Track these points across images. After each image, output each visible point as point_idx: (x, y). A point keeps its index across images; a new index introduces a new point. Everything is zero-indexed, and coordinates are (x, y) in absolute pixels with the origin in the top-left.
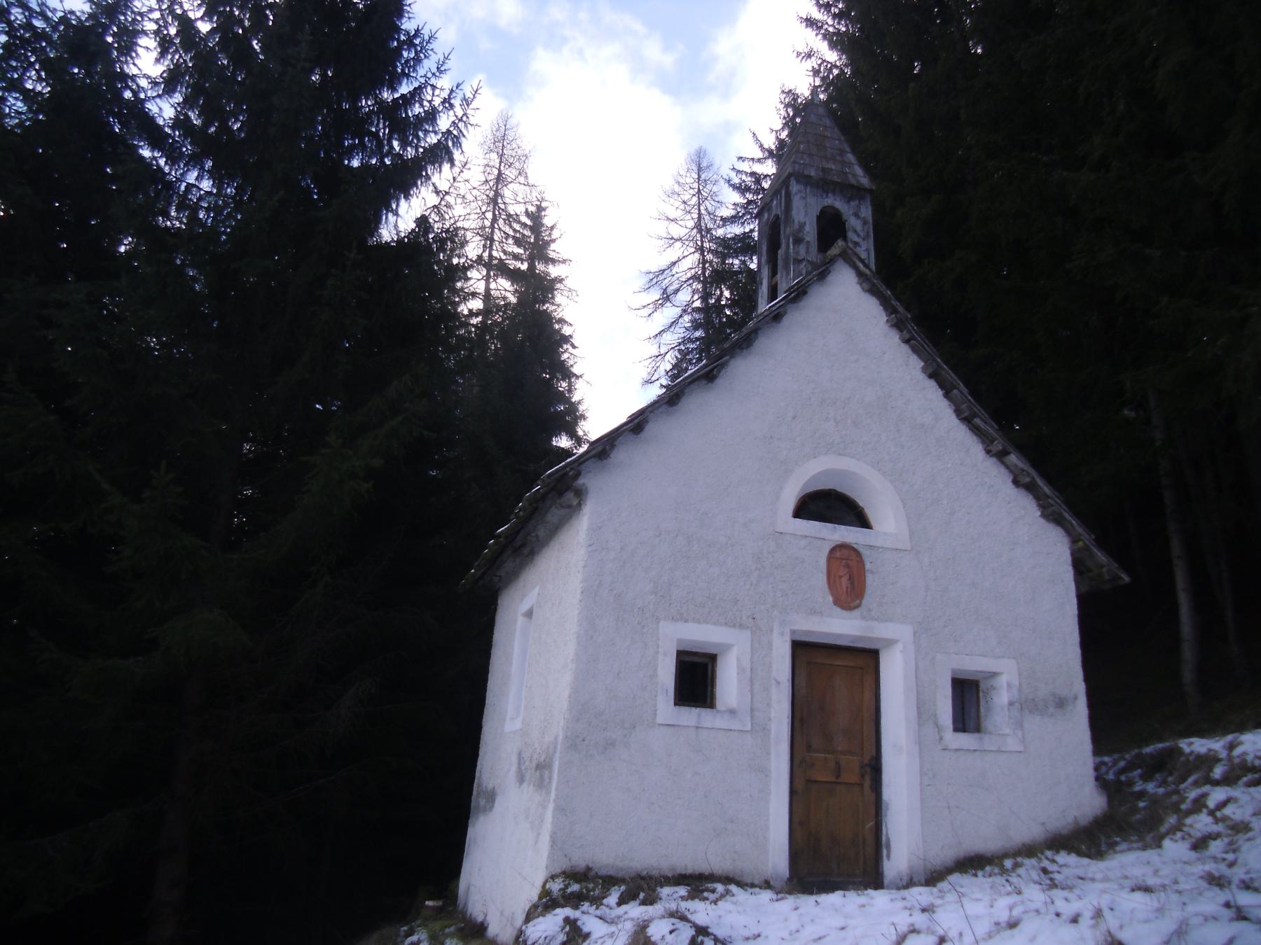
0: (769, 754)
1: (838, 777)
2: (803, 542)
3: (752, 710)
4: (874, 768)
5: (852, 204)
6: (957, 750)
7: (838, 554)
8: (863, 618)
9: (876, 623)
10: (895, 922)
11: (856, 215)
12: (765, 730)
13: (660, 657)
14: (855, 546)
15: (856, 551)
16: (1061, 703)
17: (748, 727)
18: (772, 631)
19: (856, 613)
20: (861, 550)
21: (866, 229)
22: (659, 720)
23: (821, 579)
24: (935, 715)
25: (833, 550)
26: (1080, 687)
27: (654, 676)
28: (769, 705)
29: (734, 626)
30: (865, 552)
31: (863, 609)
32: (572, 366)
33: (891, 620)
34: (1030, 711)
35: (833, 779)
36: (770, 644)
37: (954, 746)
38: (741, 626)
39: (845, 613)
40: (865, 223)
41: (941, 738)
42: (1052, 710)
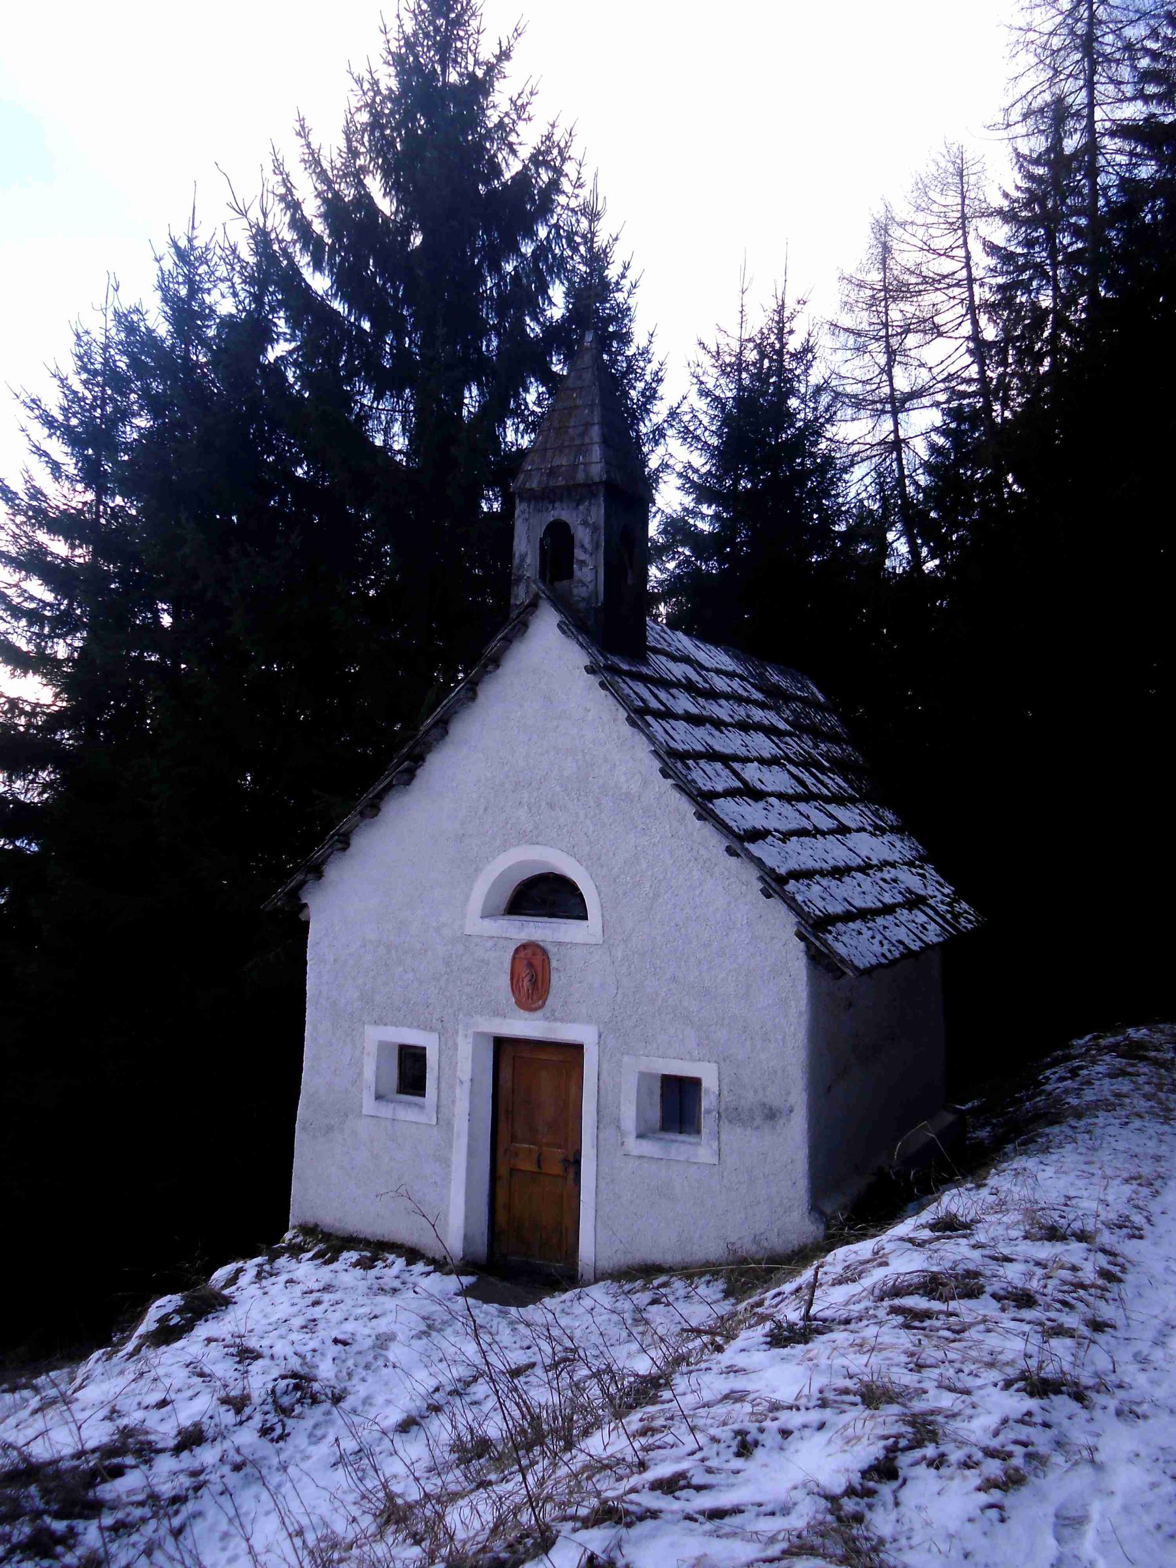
0: (451, 1147)
1: (539, 1167)
2: (490, 944)
3: (438, 1107)
4: (575, 1163)
5: (581, 508)
6: (640, 1157)
7: (522, 954)
8: (546, 1019)
9: (558, 1024)
10: (301, 1422)
11: (585, 523)
12: (449, 1124)
13: (365, 1056)
14: (541, 944)
15: (538, 946)
16: (772, 1115)
17: (434, 1122)
18: (457, 1033)
19: (539, 1013)
20: (549, 947)
21: (595, 538)
22: (364, 1112)
23: (505, 980)
24: (619, 1120)
25: (517, 951)
26: (797, 1097)
27: (360, 1074)
28: (453, 1102)
29: (425, 1029)
30: (552, 950)
31: (546, 1010)
32: (14, 670)
33: (573, 1021)
34: (730, 1122)
35: (537, 1170)
36: (455, 1045)
37: (635, 1153)
38: (432, 1029)
39: (526, 1014)
40: (595, 529)
41: (623, 1143)
42: (758, 1121)
